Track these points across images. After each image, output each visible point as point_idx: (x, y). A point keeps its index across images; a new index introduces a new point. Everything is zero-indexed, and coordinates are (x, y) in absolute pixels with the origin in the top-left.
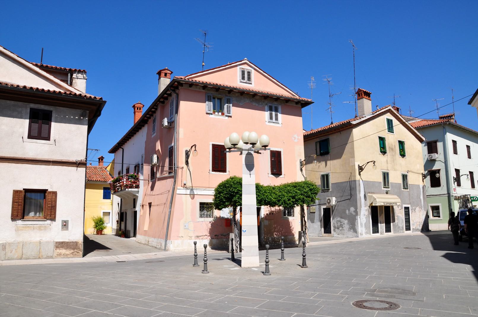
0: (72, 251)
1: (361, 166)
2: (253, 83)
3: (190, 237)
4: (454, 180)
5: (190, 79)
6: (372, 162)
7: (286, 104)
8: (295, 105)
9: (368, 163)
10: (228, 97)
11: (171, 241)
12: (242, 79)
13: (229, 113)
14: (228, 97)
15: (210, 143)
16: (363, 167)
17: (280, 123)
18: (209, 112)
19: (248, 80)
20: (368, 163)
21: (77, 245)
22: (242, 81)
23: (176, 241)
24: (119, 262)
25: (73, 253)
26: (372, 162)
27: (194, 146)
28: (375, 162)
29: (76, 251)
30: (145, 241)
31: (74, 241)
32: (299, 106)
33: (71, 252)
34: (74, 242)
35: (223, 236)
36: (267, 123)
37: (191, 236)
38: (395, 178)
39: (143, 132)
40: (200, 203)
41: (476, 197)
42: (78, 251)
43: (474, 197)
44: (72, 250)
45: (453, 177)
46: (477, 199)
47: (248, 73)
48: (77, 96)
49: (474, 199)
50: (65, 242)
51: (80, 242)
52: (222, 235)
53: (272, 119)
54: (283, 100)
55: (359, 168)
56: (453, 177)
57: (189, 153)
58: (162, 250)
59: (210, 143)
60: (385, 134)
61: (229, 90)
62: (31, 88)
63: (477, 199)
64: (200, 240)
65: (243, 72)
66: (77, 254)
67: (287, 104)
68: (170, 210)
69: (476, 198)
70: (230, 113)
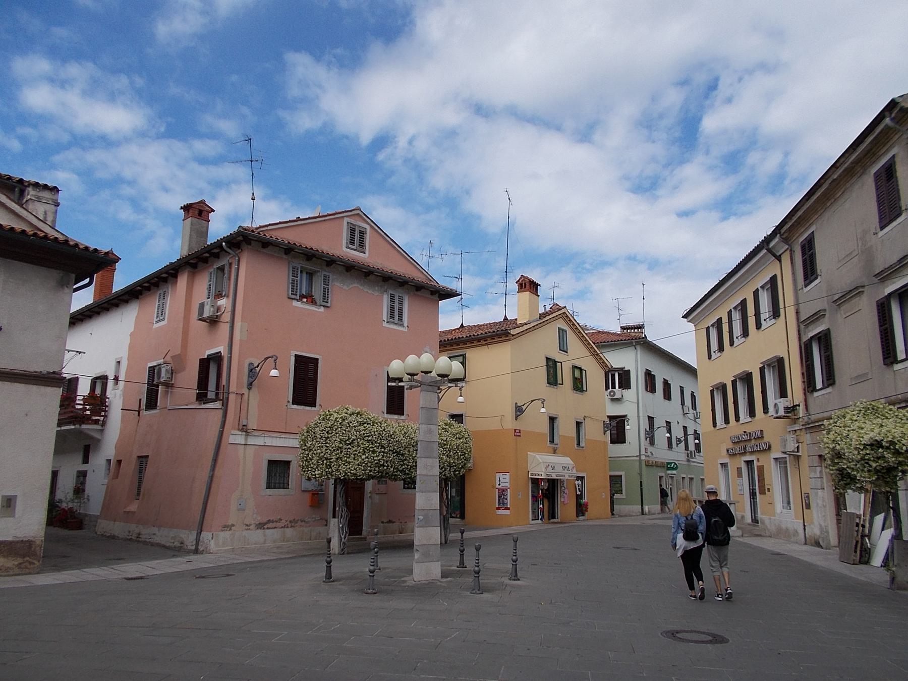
0: (20, 560)
1: (520, 405)
2: (367, 252)
3: (247, 525)
4: (677, 441)
5: (261, 233)
6: (539, 400)
7: (416, 292)
8: (430, 296)
9: (532, 401)
10: (325, 273)
11: (213, 534)
12: (350, 242)
13: (294, 294)
14: (325, 273)
15: (292, 352)
16: (524, 408)
17: (406, 325)
18: (293, 297)
19: (359, 245)
20: (532, 401)
21: (31, 547)
22: (350, 246)
23: (222, 534)
24: (132, 579)
25: (20, 564)
26: (539, 400)
27: (272, 357)
28: (544, 400)
29: (27, 561)
30: (128, 534)
31: (25, 539)
32: (436, 297)
33: (16, 563)
34: (25, 541)
35: (303, 523)
36: (385, 324)
37: (248, 524)
38: (566, 429)
39: (122, 314)
40: (269, 460)
41: (675, 464)
42: (31, 560)
43: (671, 463)
44: (18, 559)
45: (676, 437)
46: (675, 466)
47: (360, 233)
48: (90, 252)
49: (672, 466)
50: (5, 541)
51: (38, 543)
52: (302, 522)
53: (394, 317)
54: (413, 285)
55: (516, 408)
56: (676, 437)
57: (258, 369)
58: (189, 552)
59: (292, 352)
60: (558, 356)
61: (328, 260)
62: (87, 248)
63: (675, 466)
64: (265, 530)
65: (352, 231)
66: (29, 566)
67: (419, 293)
68: (211, 473)
69: (674, 466)
70: (328, 302)
